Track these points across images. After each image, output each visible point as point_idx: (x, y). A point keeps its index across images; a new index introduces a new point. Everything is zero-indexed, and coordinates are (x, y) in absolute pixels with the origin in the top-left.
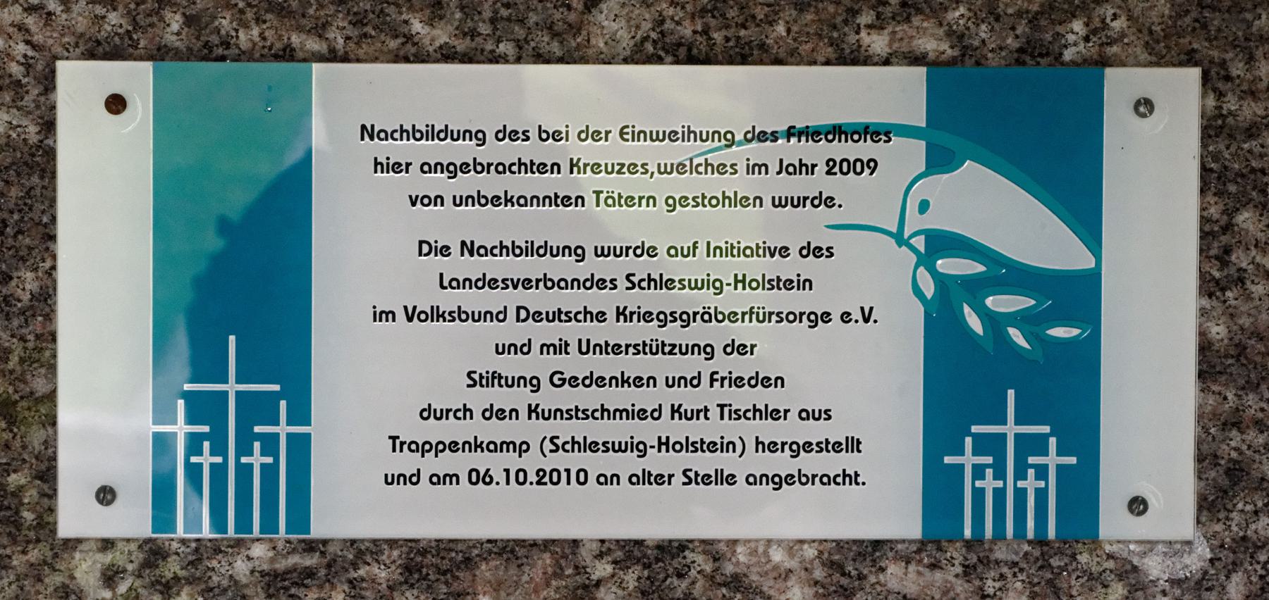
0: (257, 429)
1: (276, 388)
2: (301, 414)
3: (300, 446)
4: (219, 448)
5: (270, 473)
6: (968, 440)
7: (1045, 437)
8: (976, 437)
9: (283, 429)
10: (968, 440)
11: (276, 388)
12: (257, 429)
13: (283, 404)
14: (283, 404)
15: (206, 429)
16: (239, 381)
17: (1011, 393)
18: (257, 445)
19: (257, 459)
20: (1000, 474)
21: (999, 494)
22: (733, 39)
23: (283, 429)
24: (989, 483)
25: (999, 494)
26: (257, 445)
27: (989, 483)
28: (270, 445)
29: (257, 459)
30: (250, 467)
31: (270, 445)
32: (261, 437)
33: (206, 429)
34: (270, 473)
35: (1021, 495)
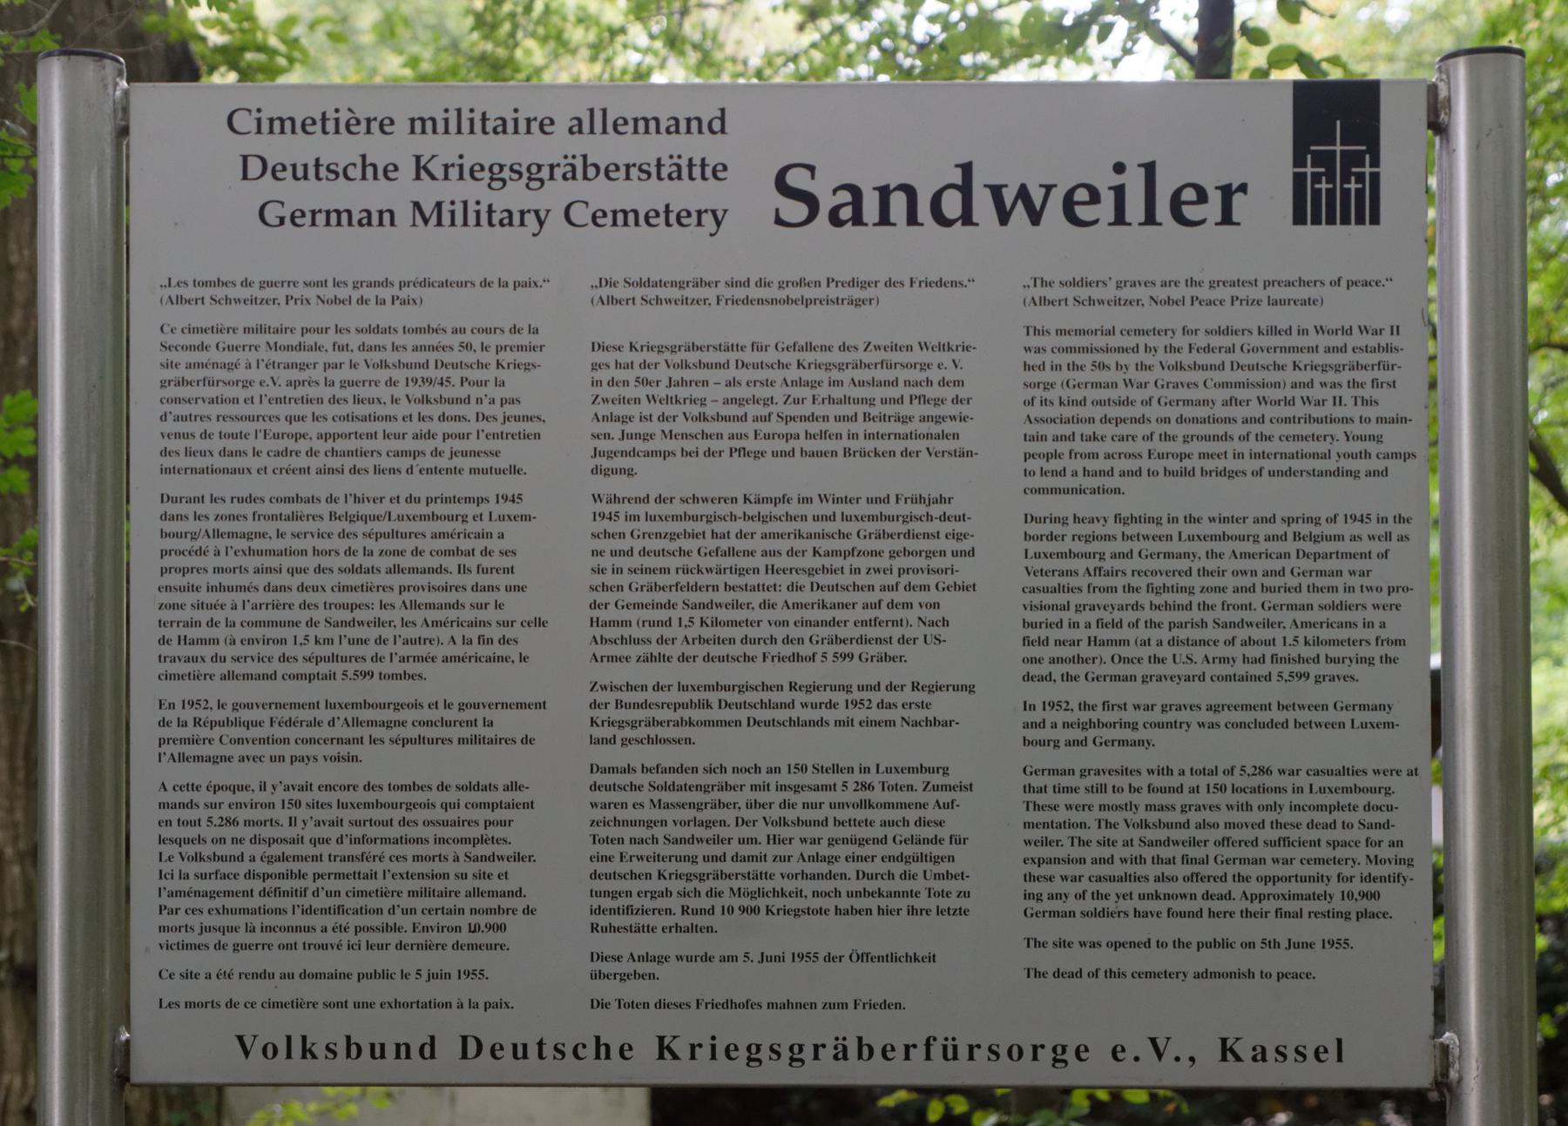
0: (1354, 170)
1: (1364, 148)
2: (1375, 162)
3: (1375, 178)
4: (1331, 180)
5: (1360, 193)
6: (1309, 157)
7: (1362, 153)
8: (1314, 153)
9: (1367, 170)
10: (1309, 157)
11: (1364, 148)
12: (1354, 170)
13: (1367, 157)
14: (1367, 157)
15: (1323, 170)
16: (1335, 145)
17: (1338, 123)
18: (1353, 178)
19: (1353, 186)
20: (1331, 180)
21: (1331, 193)
22: (367, 39)
23: (1367, 170)
24: (1324, 186)
25: (1331, 193)
26: (1353, 178)
27: (1324, 186)
28: (1360, 178)
29: (1353, 186)
30: (1349, 190)
31: (1360, 178)
32: (1355, 174)
33: (1323, 170)
34: (1360, 193)
35: (1346, 193)
